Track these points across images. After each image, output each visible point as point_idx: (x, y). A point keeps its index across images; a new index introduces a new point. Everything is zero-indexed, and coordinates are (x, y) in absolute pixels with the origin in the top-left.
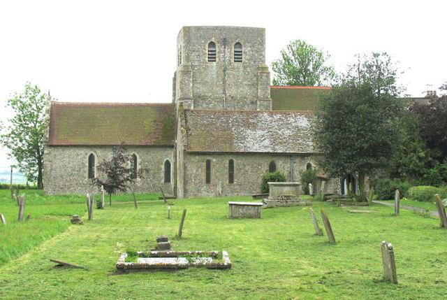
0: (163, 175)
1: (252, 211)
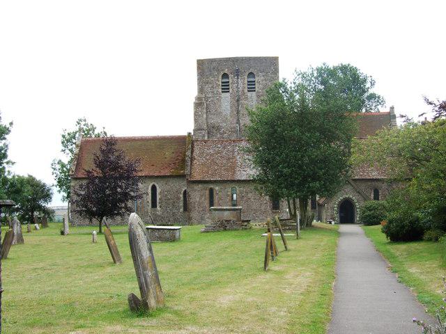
0: (181, 204)
1: (168, 235)
